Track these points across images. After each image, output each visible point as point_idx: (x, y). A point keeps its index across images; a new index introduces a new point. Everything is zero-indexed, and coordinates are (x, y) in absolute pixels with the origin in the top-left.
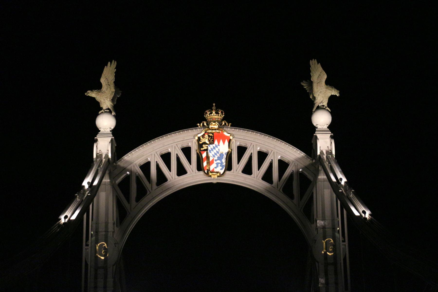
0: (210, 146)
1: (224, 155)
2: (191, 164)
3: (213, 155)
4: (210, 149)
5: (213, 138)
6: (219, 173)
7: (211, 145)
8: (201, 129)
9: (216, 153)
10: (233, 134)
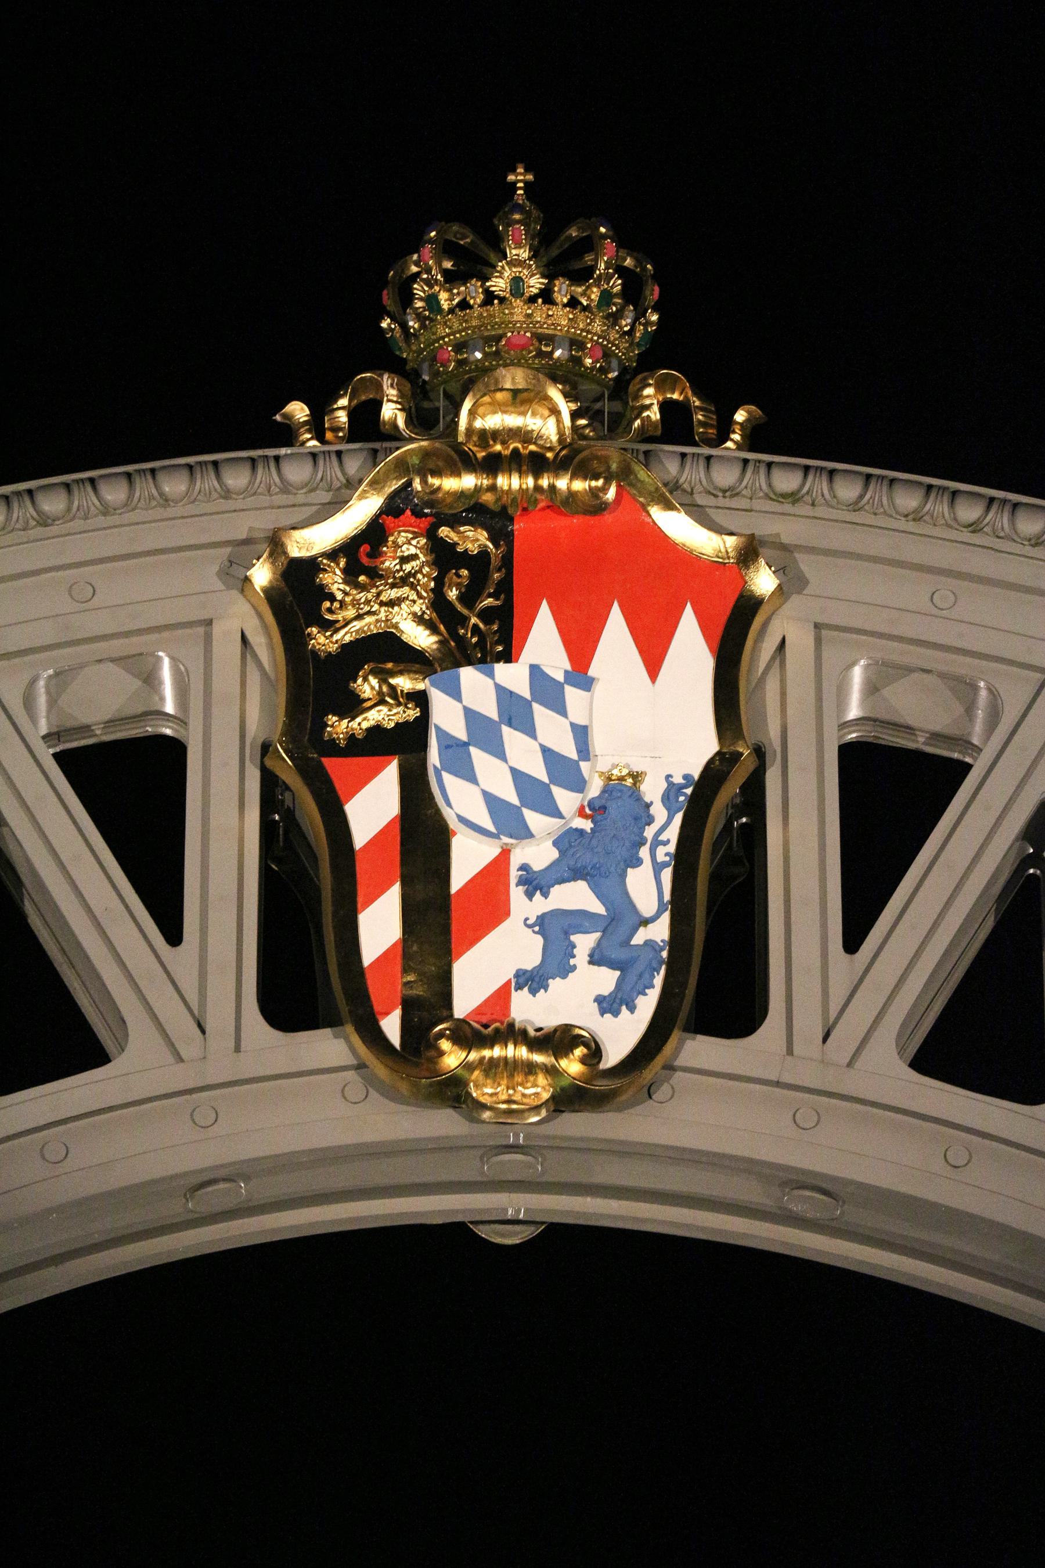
0: (455, 692)
1: (659, 812)
2: (174, 935)
3: (492, 801)
4: (459, 731)
5: (505, 588)
6: (579, 1051)
7: (468, 675)
8: (333, 471)
9: (541, 773)
10: (785, 539)
